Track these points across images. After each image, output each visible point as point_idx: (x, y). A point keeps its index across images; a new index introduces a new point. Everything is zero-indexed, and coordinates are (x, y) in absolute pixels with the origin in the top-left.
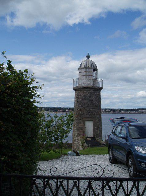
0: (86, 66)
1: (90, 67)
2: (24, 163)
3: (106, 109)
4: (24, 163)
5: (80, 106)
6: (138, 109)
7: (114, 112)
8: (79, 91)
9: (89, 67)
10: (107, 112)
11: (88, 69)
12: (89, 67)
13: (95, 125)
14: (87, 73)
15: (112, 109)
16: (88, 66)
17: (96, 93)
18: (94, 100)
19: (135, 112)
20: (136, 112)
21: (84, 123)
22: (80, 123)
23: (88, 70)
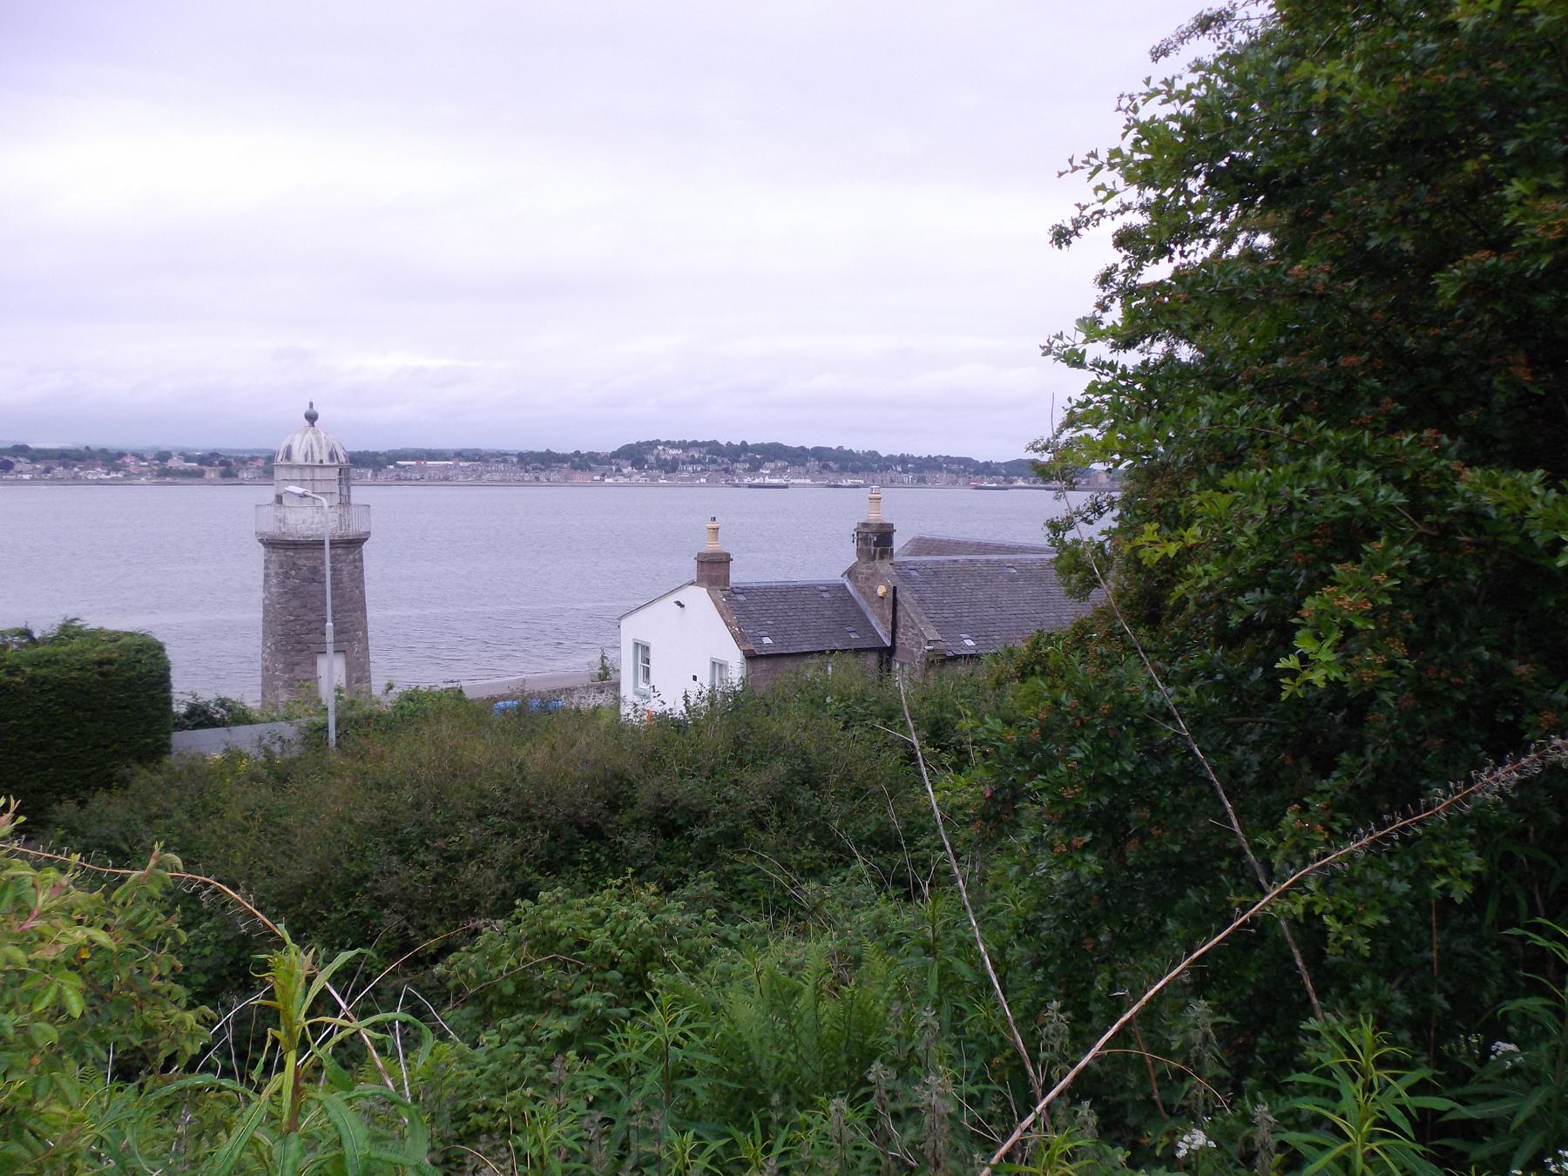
0: (313, 460)
1: (325, 463)
2: (1153, 863)
3: (164, 456)
4: (1153, 863)
5: (296, 603)
6: (393, 457)
7: (224, 475)
8: (287, 549)
9: (321, 461)
10: (166, 473)
11: (317, 471)
12: (321, 461)
13: (350, 668)
14: (317, 484)
15: (214, 455)
16: (317, 458)
17: (351, 557)
18: (345, 579)
19: (375, 475)
20: (381, 478)
21: (314, 664)
22: (298, 664)
23: (318, 474)
